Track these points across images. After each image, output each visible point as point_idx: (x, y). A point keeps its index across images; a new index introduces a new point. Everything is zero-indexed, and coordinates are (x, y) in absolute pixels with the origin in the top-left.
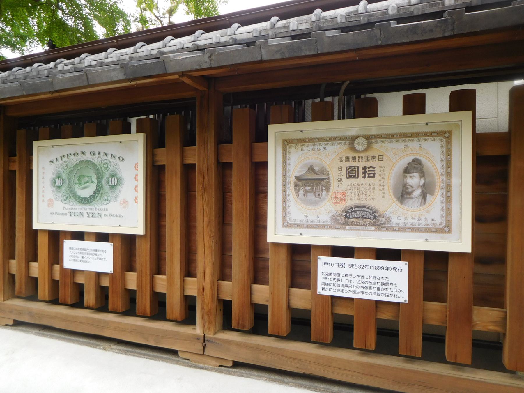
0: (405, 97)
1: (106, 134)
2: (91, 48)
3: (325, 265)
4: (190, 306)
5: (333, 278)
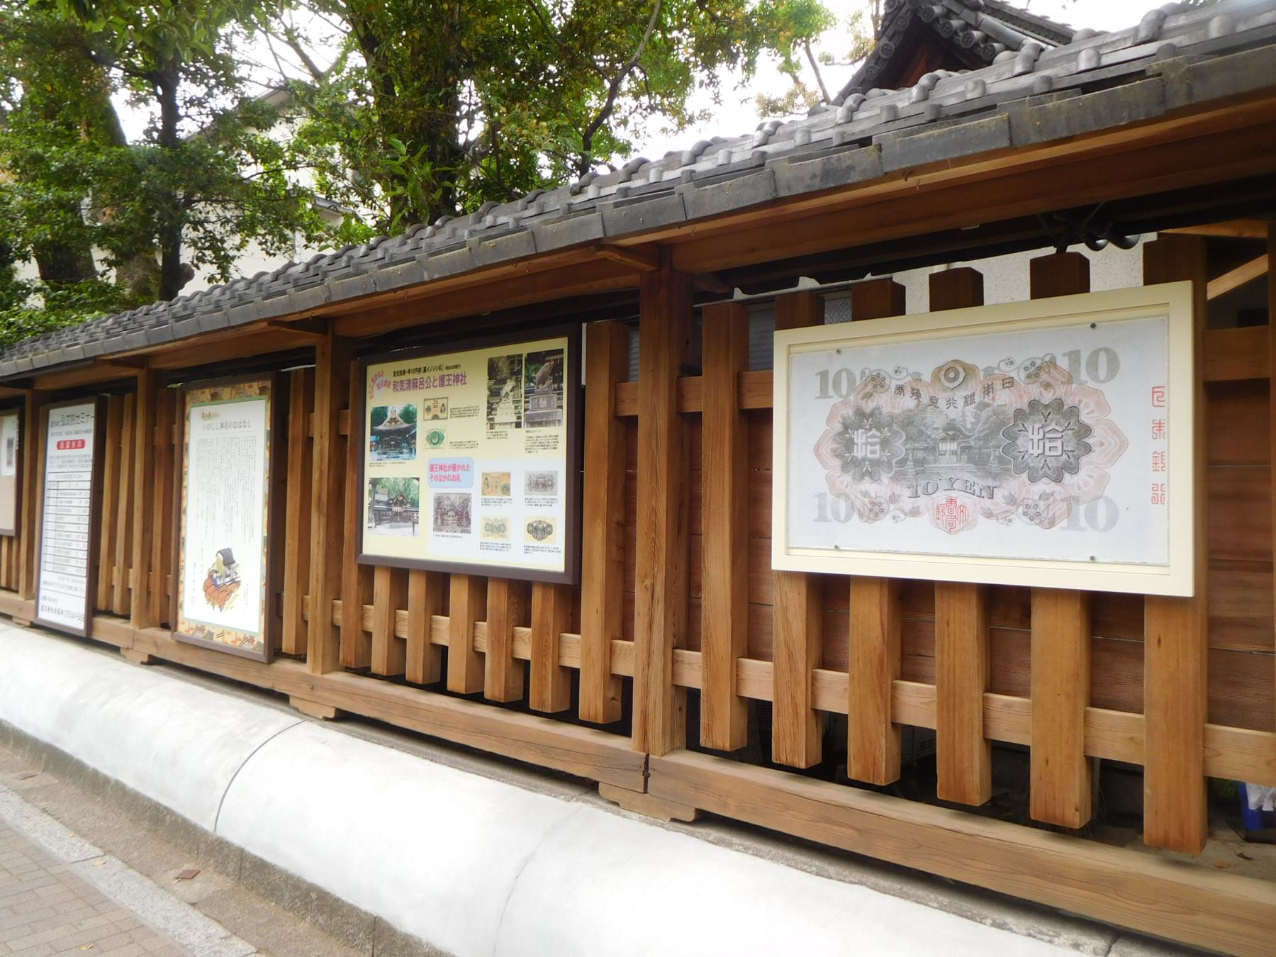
4: (832, 732)
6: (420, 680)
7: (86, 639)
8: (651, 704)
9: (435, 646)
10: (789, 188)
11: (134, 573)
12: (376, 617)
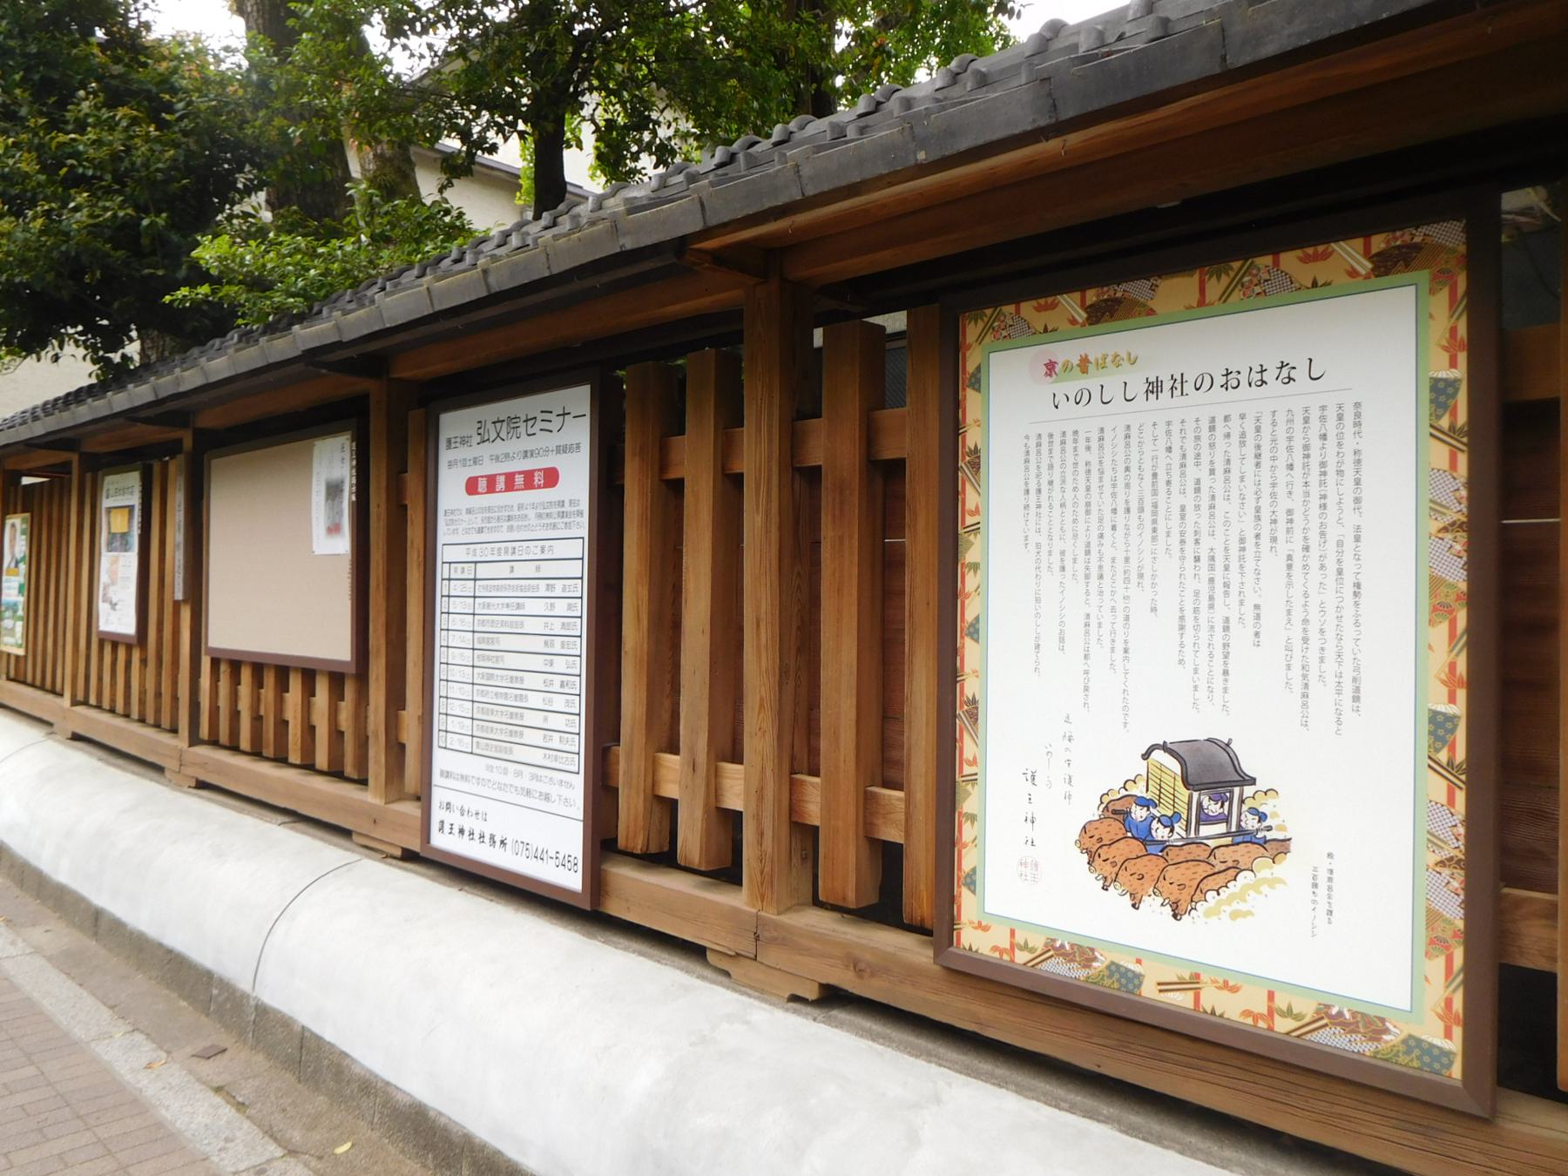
6: (298, 762)
7: (589, 912)
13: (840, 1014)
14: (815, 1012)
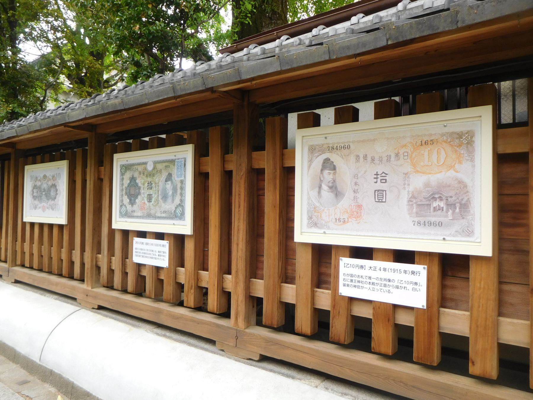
0: (298, 115)
1: (400, 115)
2: (368, 6)
3: (347, 266)
5: (357, 281)
6: (28, 266)
8: (238, 304)
9: (202, 288)
10: (463, 21)
11: (54, 249)
12: (103, 259)
13: (18, 285)
14: (97, 311)
